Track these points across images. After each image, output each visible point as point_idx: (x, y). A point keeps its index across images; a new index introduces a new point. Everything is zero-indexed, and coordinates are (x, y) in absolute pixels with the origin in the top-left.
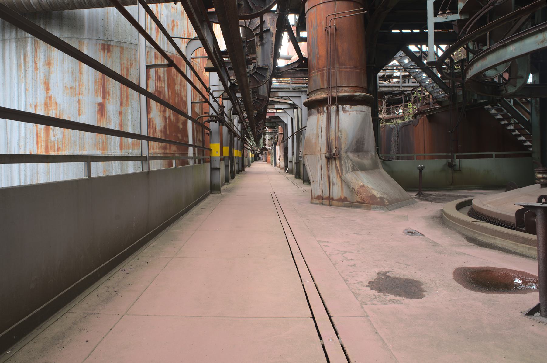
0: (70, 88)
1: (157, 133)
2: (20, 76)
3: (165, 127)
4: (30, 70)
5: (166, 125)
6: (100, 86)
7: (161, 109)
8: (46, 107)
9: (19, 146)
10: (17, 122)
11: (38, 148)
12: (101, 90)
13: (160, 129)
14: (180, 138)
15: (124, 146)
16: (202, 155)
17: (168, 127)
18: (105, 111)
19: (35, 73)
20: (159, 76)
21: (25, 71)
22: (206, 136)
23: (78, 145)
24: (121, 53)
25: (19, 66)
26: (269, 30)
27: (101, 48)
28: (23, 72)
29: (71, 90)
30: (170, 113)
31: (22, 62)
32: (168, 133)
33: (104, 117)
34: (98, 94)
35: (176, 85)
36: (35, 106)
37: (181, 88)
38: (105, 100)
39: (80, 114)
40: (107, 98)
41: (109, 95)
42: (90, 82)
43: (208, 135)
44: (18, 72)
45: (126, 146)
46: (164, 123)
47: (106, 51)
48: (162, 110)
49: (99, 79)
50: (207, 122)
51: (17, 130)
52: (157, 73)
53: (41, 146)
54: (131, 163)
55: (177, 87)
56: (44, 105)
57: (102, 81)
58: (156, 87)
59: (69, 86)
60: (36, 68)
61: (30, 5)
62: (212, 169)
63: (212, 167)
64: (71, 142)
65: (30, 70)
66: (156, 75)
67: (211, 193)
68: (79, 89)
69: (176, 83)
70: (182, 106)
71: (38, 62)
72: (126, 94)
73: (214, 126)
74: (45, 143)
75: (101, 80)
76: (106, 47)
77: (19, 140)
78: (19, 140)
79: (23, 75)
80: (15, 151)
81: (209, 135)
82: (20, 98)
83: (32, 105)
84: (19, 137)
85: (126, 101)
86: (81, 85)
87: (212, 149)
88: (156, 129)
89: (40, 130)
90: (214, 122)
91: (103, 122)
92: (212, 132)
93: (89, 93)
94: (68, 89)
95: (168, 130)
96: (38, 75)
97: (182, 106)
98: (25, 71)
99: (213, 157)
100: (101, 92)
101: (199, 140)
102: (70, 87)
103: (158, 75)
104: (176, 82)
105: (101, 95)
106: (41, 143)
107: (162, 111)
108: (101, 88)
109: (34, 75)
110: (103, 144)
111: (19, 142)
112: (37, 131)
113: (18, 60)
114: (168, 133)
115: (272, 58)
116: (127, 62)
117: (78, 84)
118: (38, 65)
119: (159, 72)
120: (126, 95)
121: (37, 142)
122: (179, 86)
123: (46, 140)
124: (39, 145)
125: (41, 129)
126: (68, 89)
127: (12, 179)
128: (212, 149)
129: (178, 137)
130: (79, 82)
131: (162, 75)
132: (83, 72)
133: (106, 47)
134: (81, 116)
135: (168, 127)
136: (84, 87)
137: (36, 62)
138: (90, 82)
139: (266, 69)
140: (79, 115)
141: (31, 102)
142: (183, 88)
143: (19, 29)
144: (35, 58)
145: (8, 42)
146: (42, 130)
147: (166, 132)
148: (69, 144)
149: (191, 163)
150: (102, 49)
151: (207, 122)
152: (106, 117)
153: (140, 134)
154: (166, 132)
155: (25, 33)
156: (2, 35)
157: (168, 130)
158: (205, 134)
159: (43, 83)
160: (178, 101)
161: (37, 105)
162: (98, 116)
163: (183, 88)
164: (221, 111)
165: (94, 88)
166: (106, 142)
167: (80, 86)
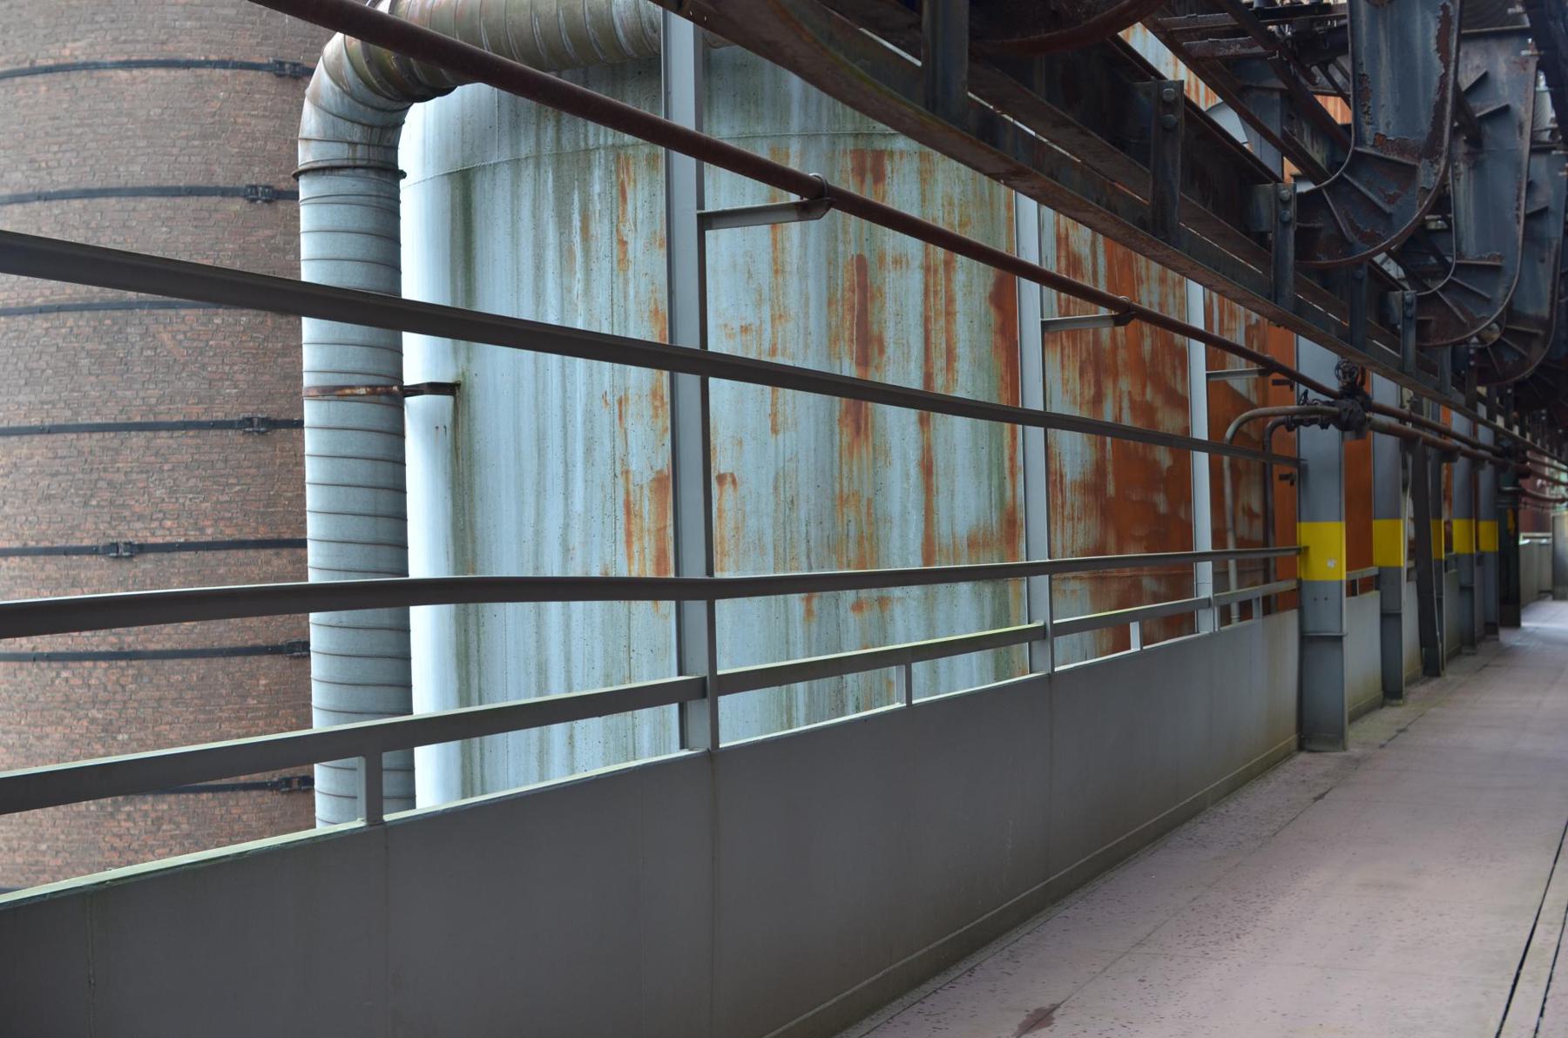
0: (741, 331)
1: (1068, 494)
2: (570, 292)
3: (1099, 470)
4: (602, 269)
5: (1103, 458)
6: (848, 317)
7: (1081, 394)
8: (658, 403)
9: (566, 550)
10: (531, 353)
11: (630, 557)
12: (852, 334)
13: (1078, 477)
14: (1163, 508)
15: (937, 549)
16: (1260, 576)
17: (1110, 468)
18: (867, 416)
19: (621, 278)
20: (1074, 255)
21: (588, 271)
22: (1280, 487)
23: (770, 548)
24: (923, 181)
25: (566, 254)
26: (1505, 110)
27: (850, 166)
28: (579, 275)
29: (744, 338)
30: (1121, 409)
31: (577, 239)
32: (1111, 489)
33: (862, 437)
34: (844, 348)
35: (1145, 285)
36: (620, 403)
37: (1166, 295)
38: (866, 371)
39: (779, 427)
40: (876, 362)
41: (882, 351)
42: (812, 304)
43: (1292, 484)
44: (561, 277)
45: (945, 551)
46: (1093, 449)
47: (869, 177)
48: (1087, 398)
49: (843, 290)
50: (1283, 427)
51: (559, 488)
52: (1067, 245)
53: (643, 549)
54: (961, 660)
55: (1150, 292)
56: (649, 398)
57: (856, 297)
58: (1063, 304)
59: (736, 325)
60: (623, 260)
61: (606, 28)
62: (1306, 640)
63: (1311, 628)
64: (744, 537)
65: (602, 269)
66: (1063, 253)
67: (1301, 747)
68: (773, 333)
69: (1144, 278)
70: (1168, 372)
71: (630, 237)
72: (947, 341)
73: (1319, 443)
74: (657, 541)
75: (853, 291)
76: (869, 163)
77: (566, 527)
78: (566, 527)
79: (578, 287)
80: (553, 568)
81: (1296, 483)
82: (567, 371)
83: (609, 398)
84: (567, 514)
85: (944, 372)
86: (780, 316)
87: (1307, 548)
88: (1061, 476)
89: (637, 489)
90: (1316, 428)
91: (860, 457)
92: (1306, 467)
93: (806, 346)
94: (734, 335)
95: (1110, 478)
96: (631, 285)
97: (1168, 372)
98: (588, 271)
99: (1313, 582)
100: (852, 341)
101: (1250, 513)
102: (742, 327)
103: (1068, 253)
104: (1143, 272)
105: (852, 352)
106: (641, 539)
107: (1088, 402)
108: (852, 325)
109: (618, 286)
110: (860, 543)
111: (567, 535)
112: (628, 493)
113: (561, 234)
114: (1111, 489)
115: (1518, 222)
116: (949, 213)
117: (766, 312)
118: (630, 247)
119: (1072, 239)
120: (944, 346)
121: (629, 534)
122: (1155, 286)
123: (659, 530)
124: (636, 547)
125: (642, 487)
126: (734, 335)
127: (542, 670)
128: (1307, 548)
129: (1154, 506)
130: (772, 308)
131: (1085, 251)
132: (788, 268)
133: (869, 163)
134: (780, 436)
135: (1110, 468)
136: (791, 325)
137: (625, 239)
138: (812, 304)
139: (1495, 270)
140: (775, 431)
141: (607, 387)
142: (1174, 296)
143: (566, 116)
144: (618, 222)
145: (531, 167)
146: (646, 491)
147: (1105, 485)
148: (737, 545)
149: (1207, 623)
150: (853, 170)
151: (1283, 427)
152: (870, 438)
153: (1044, 287)
154: (1105, 489)
155: (586, 125)
156: (512, 145)
157: (1110, 478)
158: (1276, 478)
159: (646, 315)
160: (1154, 352)
161: (627, 399)
162: (841, 434)
163: (1174, 296)
164: (1348, 379)
165: (829, 325)
166: (872, 535)
167: (777, 322)
